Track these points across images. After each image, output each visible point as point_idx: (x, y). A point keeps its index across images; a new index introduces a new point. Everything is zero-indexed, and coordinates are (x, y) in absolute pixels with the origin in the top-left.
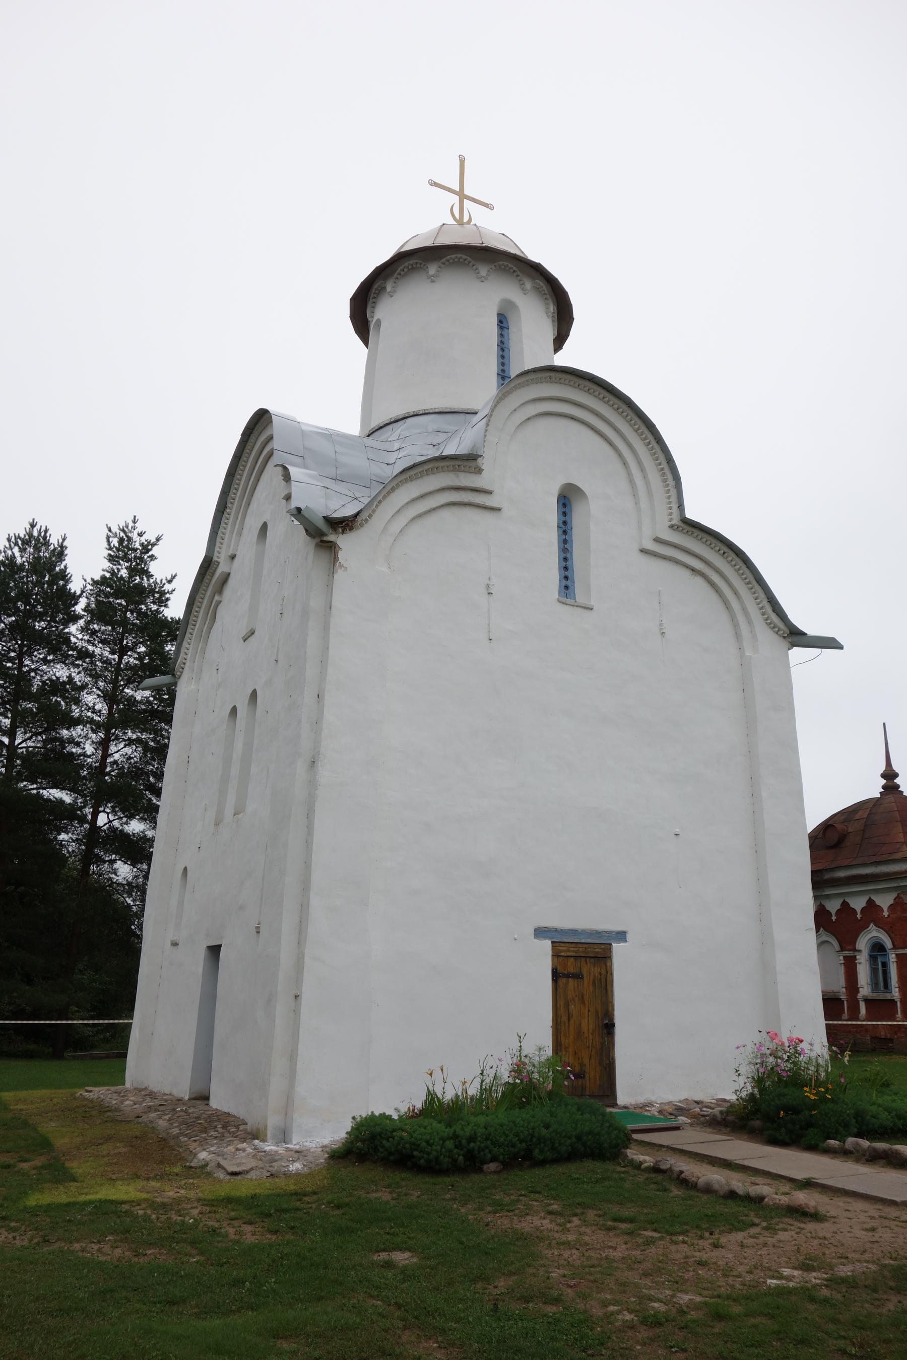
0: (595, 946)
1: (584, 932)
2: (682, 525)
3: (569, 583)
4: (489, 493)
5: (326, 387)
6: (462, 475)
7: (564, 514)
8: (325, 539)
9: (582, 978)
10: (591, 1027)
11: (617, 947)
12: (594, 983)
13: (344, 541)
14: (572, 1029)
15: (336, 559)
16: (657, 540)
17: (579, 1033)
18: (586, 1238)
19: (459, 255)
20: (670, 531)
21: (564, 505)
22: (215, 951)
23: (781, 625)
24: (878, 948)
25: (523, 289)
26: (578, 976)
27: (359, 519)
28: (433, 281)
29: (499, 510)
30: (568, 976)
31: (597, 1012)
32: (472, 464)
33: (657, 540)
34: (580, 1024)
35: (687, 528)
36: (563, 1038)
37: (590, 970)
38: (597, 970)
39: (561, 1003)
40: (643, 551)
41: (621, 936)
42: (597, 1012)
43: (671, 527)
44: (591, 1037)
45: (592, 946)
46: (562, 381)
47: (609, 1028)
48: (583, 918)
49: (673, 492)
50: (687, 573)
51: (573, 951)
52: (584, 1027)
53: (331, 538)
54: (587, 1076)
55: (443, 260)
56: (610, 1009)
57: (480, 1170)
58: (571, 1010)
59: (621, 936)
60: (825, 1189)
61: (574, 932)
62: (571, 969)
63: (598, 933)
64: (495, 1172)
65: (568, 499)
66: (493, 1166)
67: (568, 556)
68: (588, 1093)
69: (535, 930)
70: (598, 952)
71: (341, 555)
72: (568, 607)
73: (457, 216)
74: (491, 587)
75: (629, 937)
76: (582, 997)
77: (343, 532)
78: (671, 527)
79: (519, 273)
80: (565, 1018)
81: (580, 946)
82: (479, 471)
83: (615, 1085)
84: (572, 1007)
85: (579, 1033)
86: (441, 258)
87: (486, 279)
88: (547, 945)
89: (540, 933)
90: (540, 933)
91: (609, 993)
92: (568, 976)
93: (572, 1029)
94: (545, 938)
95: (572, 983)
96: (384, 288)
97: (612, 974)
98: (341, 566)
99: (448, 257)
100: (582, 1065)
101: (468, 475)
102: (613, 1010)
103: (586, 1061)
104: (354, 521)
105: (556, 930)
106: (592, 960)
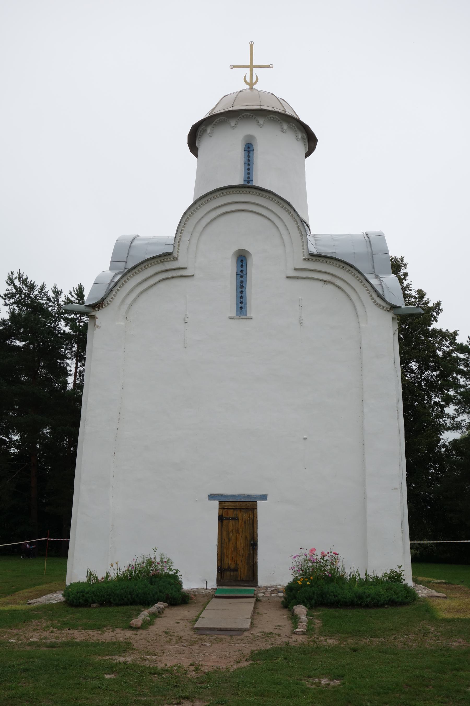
0: (247, 503)
1: (239, 496)
2: (310, 257)
3: (242, 305)
6: (166, 264)
7: (242, 266)
8: (90, 315)
9: (238, 519)
10: (242, 545)
12: (245, 523)
13: (99, 314)
14: (231, 546)
15: (95, 323)
16: (296, 269)
17: (235, 549)
19: (221, 118)
20: (305, 262)
21: (242, 261)
23: (384, 304)
25: (259, 125)
26: (235, 519)
27: (105, 302)
28: (211, 136)
29: (193, 276)
31: (246, 538)
32: (171, 256)
33: (296, 269)
34: (236, 544)
35: (314, 258)
36: (225, 551)
37: (242, 516)
38: (246, 516)
39: (225, 533)
41: (264, 497)
42: (246, 538)
43: (304, 259)
44: (242, 550)
45: (245, 503)
46: (231, 192)
47: (254, 546)
50: (321, 284)
51: (233, 506)
52: (239, 545)
53: (93, 313)
54: (239, 570)
55: (214, 123)
56: (255, 536)
57: (90, 606)
58: (230, 536)
59: (264, 497)
60: (280, 626)
61: (234, 496)
63: (249, 496)
64: (95, 608)
65: (242, 258)
66: (95, 605)
67: (243, 290)
68: (239, 579)
69: (209, 496)
70: (248, 506)
71: (97, 321)
72: (236, 320)
73: (248, 80)
74: (186, 319)
75: (268, 498)
76: (238, 530)
77: (99, 309)
78: (304, 259)
79: (255, 116)
80: (227, 540)
81: (237, 503)
82: (177, 259)
83: (257, 576)
84: (231, 535)
85: (235, 549)
86: (212, 123)
87: (236, 127)
88: (216, 503)
89: (212, 497)
90: (212, 497)
91: (255, 527)
93: (231, 546)
94: (215, 499)
95: (231, 522)
97: (257, 518)
98: (98, 326)
99: (216, 121)
100: (236, 564)
101: (170, 262)
102: (257, 536)
103: (239, 562)
104: (103, 303)
105: (222, 495)
106: (244, 510)
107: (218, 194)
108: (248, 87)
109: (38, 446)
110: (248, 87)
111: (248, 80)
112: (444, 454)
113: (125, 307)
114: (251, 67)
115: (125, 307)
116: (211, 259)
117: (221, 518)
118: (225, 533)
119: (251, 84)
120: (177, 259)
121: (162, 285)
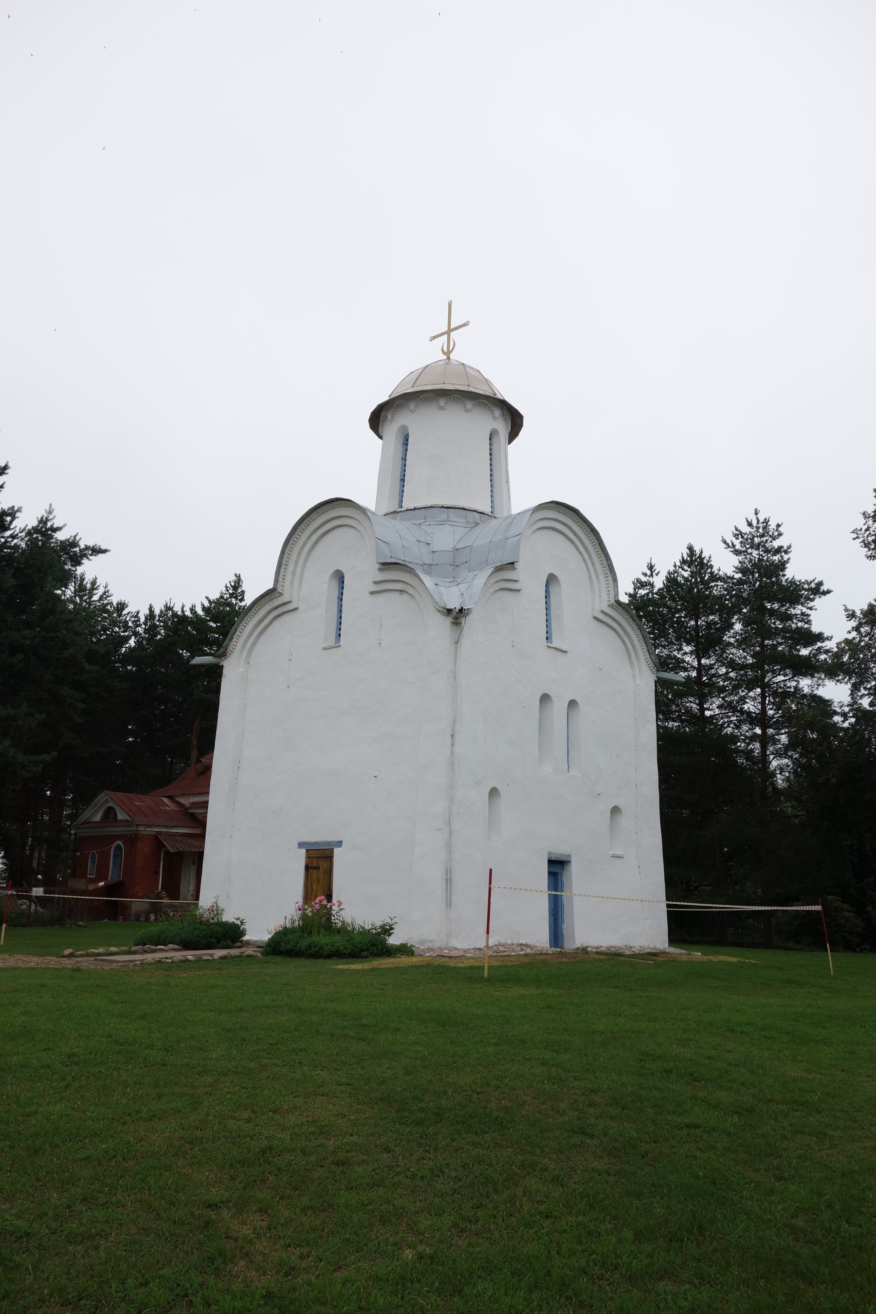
4: (290, 602)
5: (357, 469)
11: (336, 851)
16: (602, 612)
18: (647, 1066)
22: (557, 867)
24: (118, 848)
26: (317, 868)
30: (312, 868)
33: (376, 583)
37: (323, 865)
39: (309, 883)
40: (595, 618)
41: (339, 844)
48: (319, 836)
49: (612, 589)
50: (397, 594)
59: (339, 844)
62: (315, 865)
73: (445, 350)
88: (304, 851)
89: (301, 845)
90: (301, 845)
92: (312, 868)
96: (386, 417)
107: (314, 515)
108: (445, 357)
109: (49, 792)
110: (445, 357)
111: (445, 350)
112: (787, 793)
113: (245, 652)
114: (450, 331)
115: (245, 652)
116: (311, 589)
117: (307, 868)
118: (309, 883)
119: (448, 353)
120: (281, 594)
121: (276, 624)
